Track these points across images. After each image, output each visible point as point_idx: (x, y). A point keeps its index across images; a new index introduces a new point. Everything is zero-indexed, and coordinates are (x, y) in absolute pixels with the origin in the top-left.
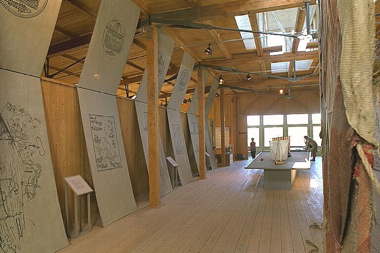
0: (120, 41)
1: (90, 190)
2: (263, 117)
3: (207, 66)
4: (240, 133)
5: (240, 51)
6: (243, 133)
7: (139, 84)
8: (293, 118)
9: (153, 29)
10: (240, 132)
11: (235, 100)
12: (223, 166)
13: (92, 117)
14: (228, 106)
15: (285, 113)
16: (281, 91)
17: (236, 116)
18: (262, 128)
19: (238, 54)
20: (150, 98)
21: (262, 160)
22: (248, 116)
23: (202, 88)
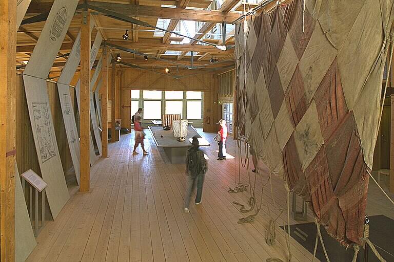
0: (61, 26)
1: (23, 175)
2: (143, 92)
3: (113, 46)
4: (123, 107)
5: (150, 37)
6: (126, 107)
7: (30, 55)
8: (169, 94)
9: (89, 15)
10: (125, 105)
11: (120, 73)
12: (113, 142)
13: (35, 105)
14: (291, 166)
15: (163, 89)
16: (167, 70)
17: (121, 89)
18: (142, 100)
19: (148, 39)
20: (83, 83)
21: (162, 137)
22: (132, 91)
23: (106, 67)
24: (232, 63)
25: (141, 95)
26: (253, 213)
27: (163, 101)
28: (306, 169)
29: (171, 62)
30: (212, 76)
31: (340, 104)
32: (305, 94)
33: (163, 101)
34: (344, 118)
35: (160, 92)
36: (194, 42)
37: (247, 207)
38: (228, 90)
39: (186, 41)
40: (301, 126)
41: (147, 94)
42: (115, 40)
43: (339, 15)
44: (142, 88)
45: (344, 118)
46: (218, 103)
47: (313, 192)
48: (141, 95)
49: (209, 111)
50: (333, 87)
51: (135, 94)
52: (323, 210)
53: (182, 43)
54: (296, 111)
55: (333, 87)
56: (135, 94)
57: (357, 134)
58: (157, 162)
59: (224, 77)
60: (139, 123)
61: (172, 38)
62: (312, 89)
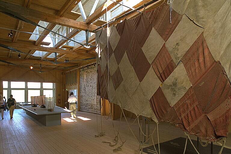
8: (31, 85)
15: (27, 81)
16: (32, 68)
24: (77, 65)
25: (9, 85)
26: (118, 145)
27: (26, 90)
28: (174, 106)
29: (36, 62)
30: (61, 73)
31: (207, 59)
32: (172, 60)
33: (26, 90)
34: (210, 68)
35: (4, 91)
36: (56, 47)
37: (113, 144)
38: (73, 82)
39: (51, 46)
40: (169, 81)
41: (14, 84)
42: (114, 8)
43: (205, 7)
44: (9, 81)
45: (210, 68)
46: (65, 90)
47: (183, 117)
48: (9, 85)
49: (59, 95)
50: (201, 50)
51: (5, 84)
52: (193, 125)
53: (49, 46)
54: (163, 72)
55: (201, 50)
56: (5, 84)
57: (224, 73)
58: (28, 125)
59: (72, 73)
60: (12, 104)
61: (43, 42)
62: (178, 56)
